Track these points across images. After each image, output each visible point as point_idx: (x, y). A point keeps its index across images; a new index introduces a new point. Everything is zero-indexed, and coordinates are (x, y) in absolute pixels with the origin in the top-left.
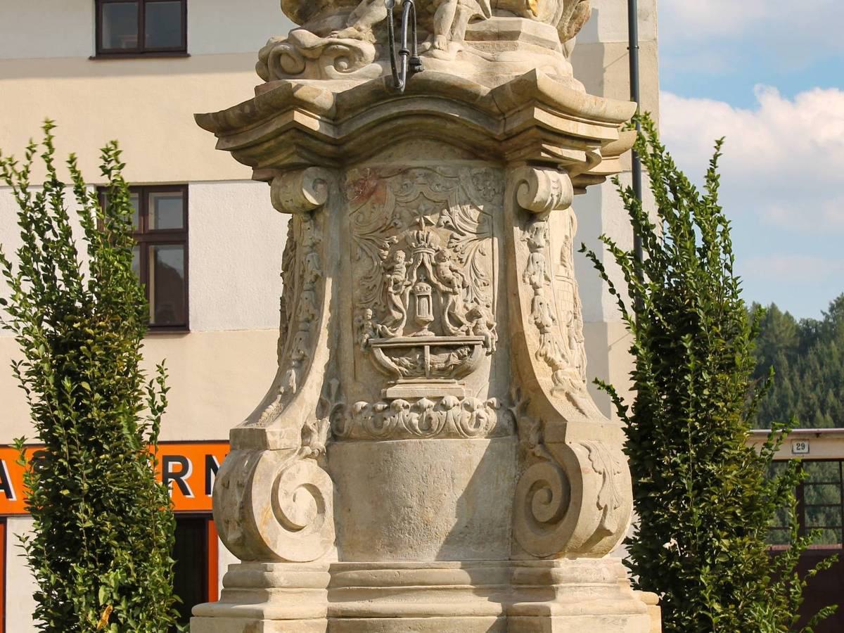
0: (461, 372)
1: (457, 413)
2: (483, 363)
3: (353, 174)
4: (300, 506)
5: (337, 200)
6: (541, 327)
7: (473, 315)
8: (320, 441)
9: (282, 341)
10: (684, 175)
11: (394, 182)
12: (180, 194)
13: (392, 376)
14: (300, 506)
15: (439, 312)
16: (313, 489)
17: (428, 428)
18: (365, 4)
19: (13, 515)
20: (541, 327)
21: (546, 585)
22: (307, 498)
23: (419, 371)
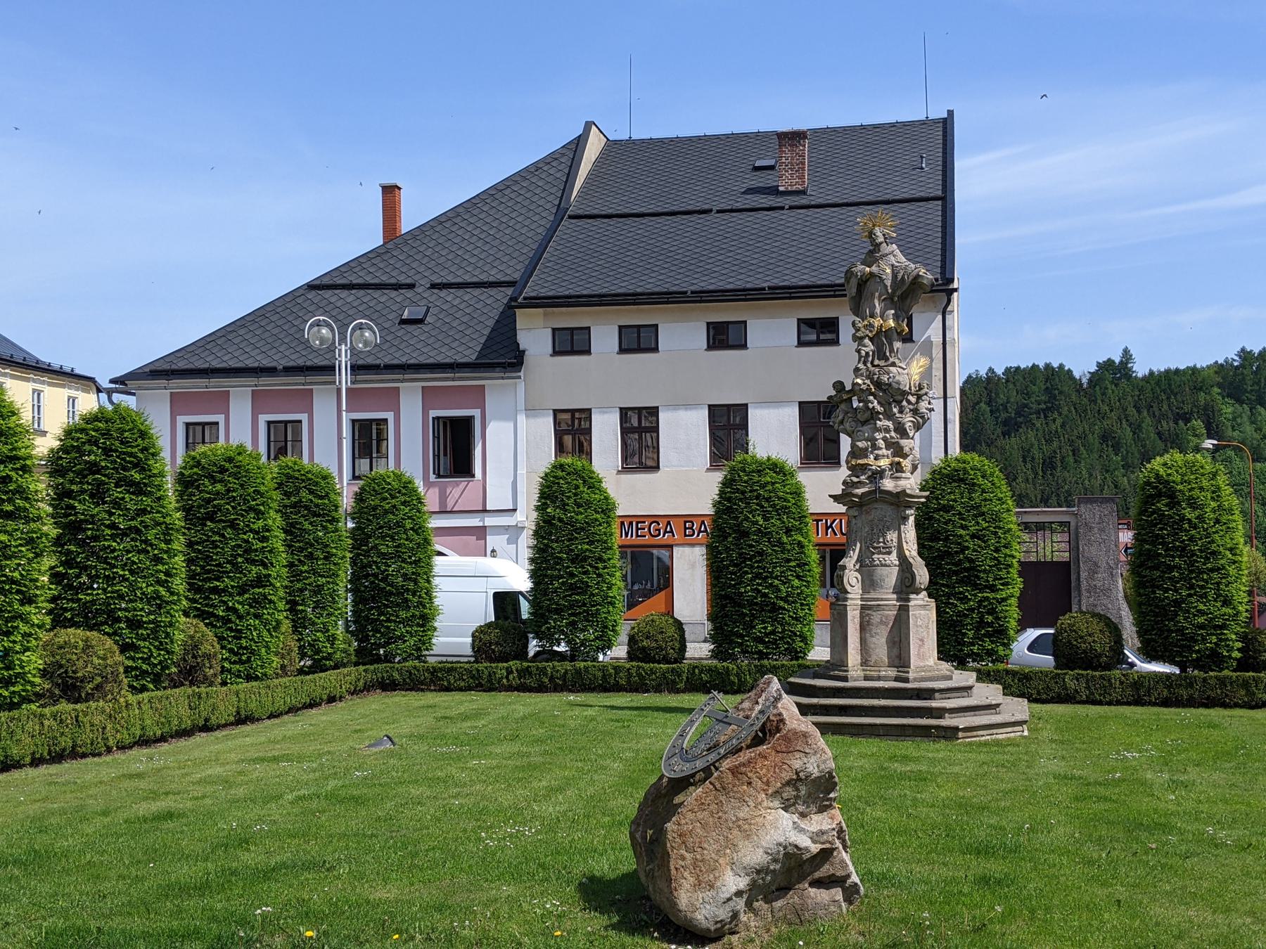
0: (889, 553)
1: (888, 562)
2: (894, 554)
3: (864, 509)
4: (854, 581)
5: (861, 514)
6: (907, 543)
7: (892, 540)
8: (857, 567)
9: (1225, 706)
10: (1055, 365)
11: (874, 511)
12: (587, 331)
13: (874, 554)
14: (854, 581)
15: (884, 539)
16: (857, 578)
17: (882, 565)
18: (980, 871)
19: (677, 545)
20: (907, 543)
21: (908, 600)
22: (855, 580)
23: (880, 553)
